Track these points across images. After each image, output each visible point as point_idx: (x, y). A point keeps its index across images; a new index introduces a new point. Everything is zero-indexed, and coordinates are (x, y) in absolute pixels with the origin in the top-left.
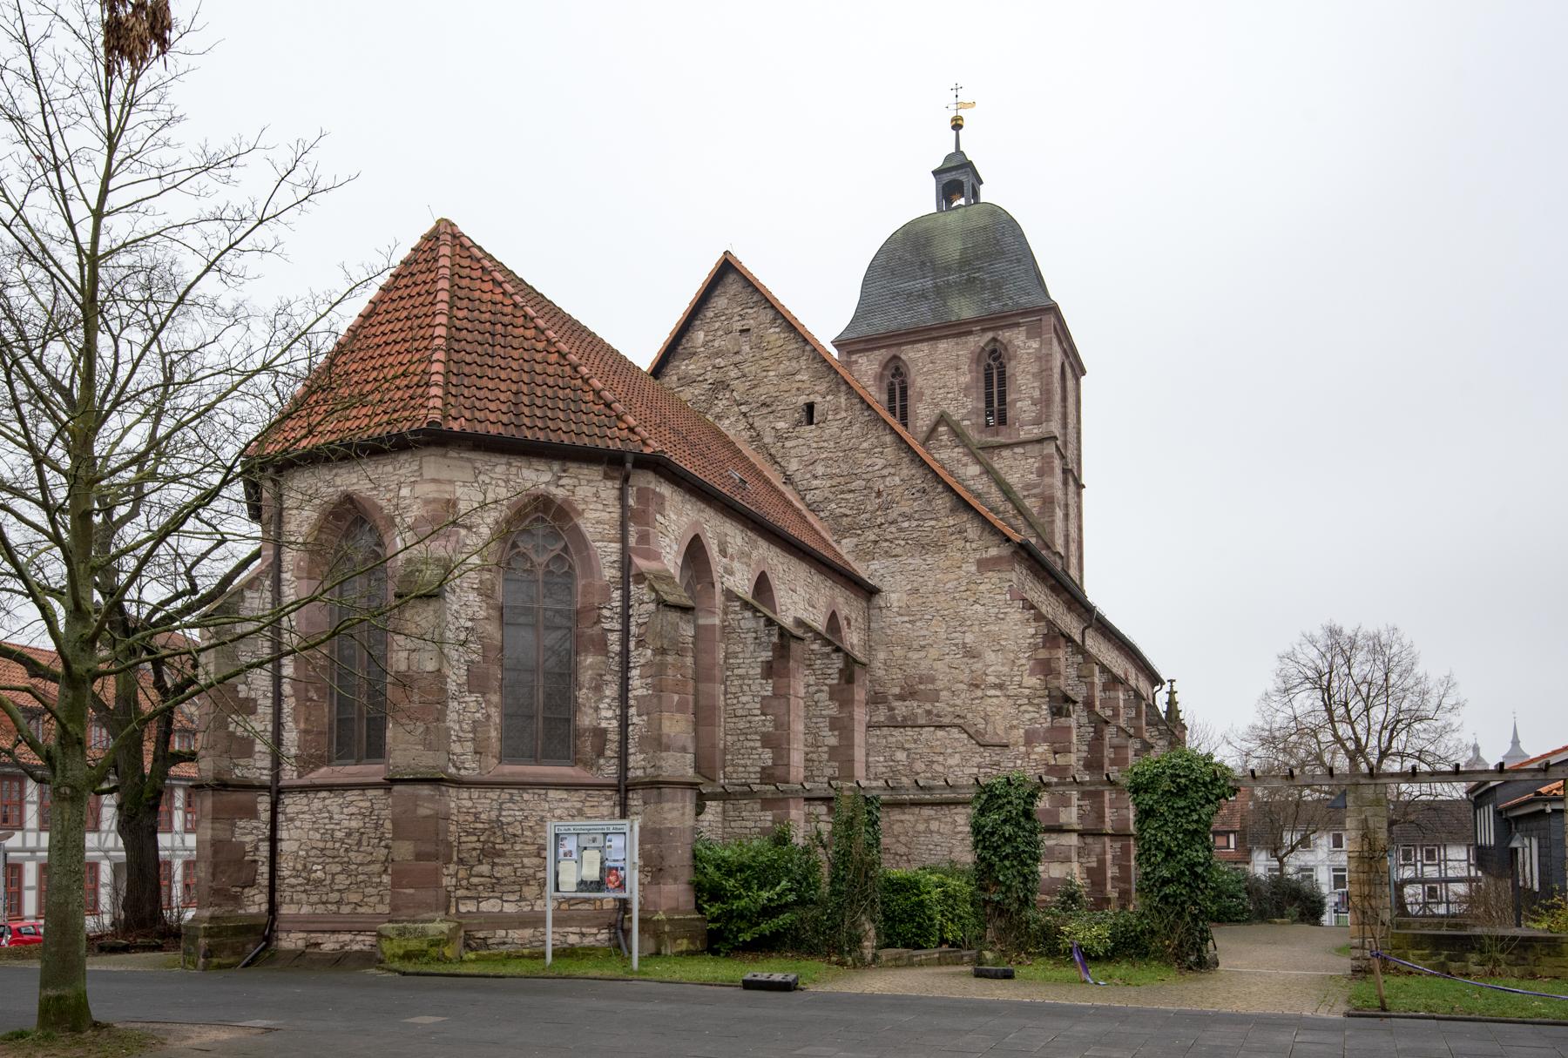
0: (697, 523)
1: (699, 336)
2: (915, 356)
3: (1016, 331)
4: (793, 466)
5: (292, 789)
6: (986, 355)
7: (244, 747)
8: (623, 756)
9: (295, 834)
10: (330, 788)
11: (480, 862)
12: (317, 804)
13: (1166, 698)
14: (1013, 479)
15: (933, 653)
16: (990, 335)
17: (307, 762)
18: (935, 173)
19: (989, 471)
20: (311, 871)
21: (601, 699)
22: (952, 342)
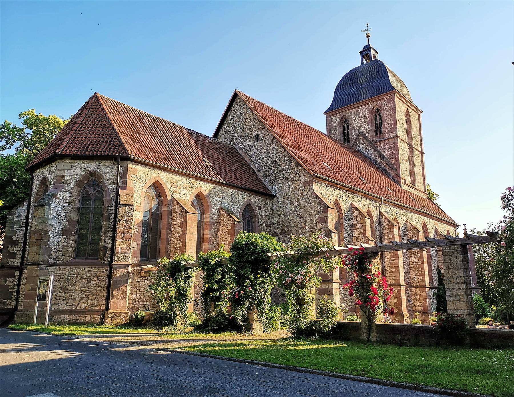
1: (230, 117)
2: (351, 114)
7: (13, 255)
11: (60, 292)
13: (463, 231)
14: (385, 153)
15: (291, 217)
16: (375, 103)
19: (377, 151)
21: (106, 237)
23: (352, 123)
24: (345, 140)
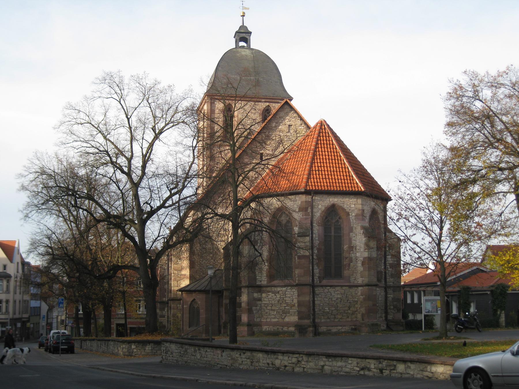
5: (318, 286)
9: (319, 299)
10: (331, 286)
12: (326, 290)
16: (268, 104)
17: (321, 279)
20: (325, 309)
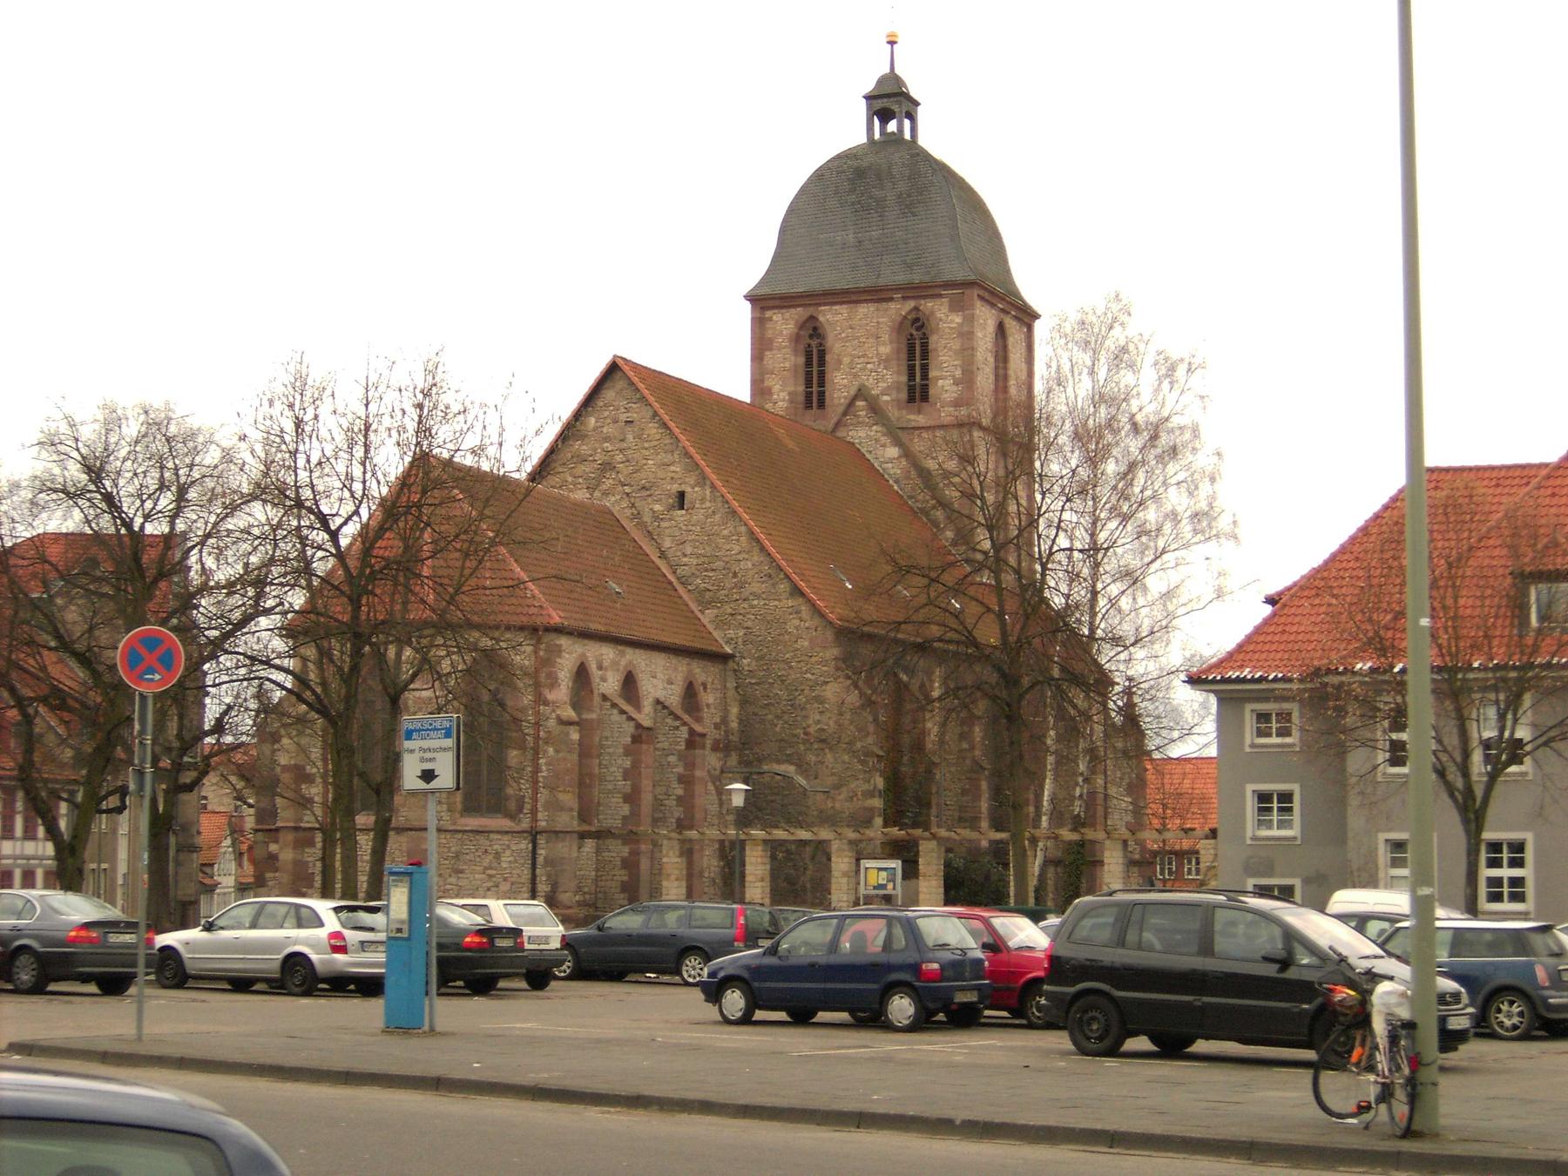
0: (583, 655)
2: (833, 318)
3: (938, 301)
4: (667, 543)
6: (908, 323)
8: (534, 812)
16: (911, 304)
18: (868, 98)
19: (907, 454)
22: (872, 307)
23: (837, 346)
24: (808, 396)
